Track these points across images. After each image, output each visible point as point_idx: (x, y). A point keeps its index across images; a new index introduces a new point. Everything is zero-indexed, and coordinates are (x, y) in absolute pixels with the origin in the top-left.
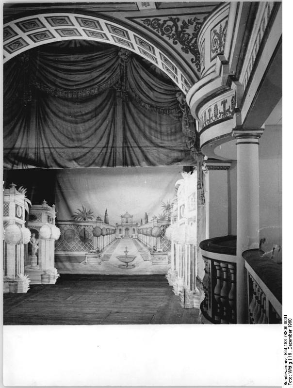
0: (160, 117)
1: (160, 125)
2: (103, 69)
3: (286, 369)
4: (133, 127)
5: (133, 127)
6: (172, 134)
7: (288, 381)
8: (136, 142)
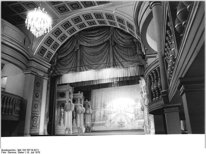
0: (128, 50)
1: (128, 53)
2: (105, 34)
3: (10, 150)
4: (118, 56)
5: (118, 56)
6: (134, 55)
7: (4, 151)
8: (118, 60)
